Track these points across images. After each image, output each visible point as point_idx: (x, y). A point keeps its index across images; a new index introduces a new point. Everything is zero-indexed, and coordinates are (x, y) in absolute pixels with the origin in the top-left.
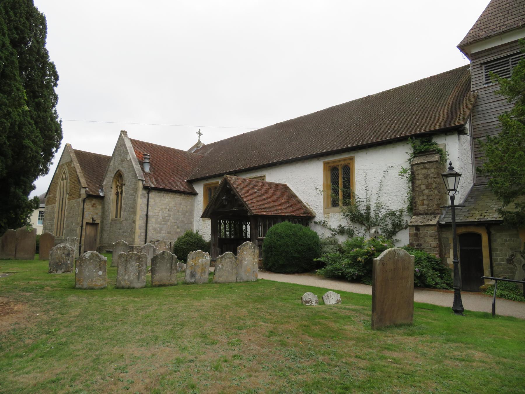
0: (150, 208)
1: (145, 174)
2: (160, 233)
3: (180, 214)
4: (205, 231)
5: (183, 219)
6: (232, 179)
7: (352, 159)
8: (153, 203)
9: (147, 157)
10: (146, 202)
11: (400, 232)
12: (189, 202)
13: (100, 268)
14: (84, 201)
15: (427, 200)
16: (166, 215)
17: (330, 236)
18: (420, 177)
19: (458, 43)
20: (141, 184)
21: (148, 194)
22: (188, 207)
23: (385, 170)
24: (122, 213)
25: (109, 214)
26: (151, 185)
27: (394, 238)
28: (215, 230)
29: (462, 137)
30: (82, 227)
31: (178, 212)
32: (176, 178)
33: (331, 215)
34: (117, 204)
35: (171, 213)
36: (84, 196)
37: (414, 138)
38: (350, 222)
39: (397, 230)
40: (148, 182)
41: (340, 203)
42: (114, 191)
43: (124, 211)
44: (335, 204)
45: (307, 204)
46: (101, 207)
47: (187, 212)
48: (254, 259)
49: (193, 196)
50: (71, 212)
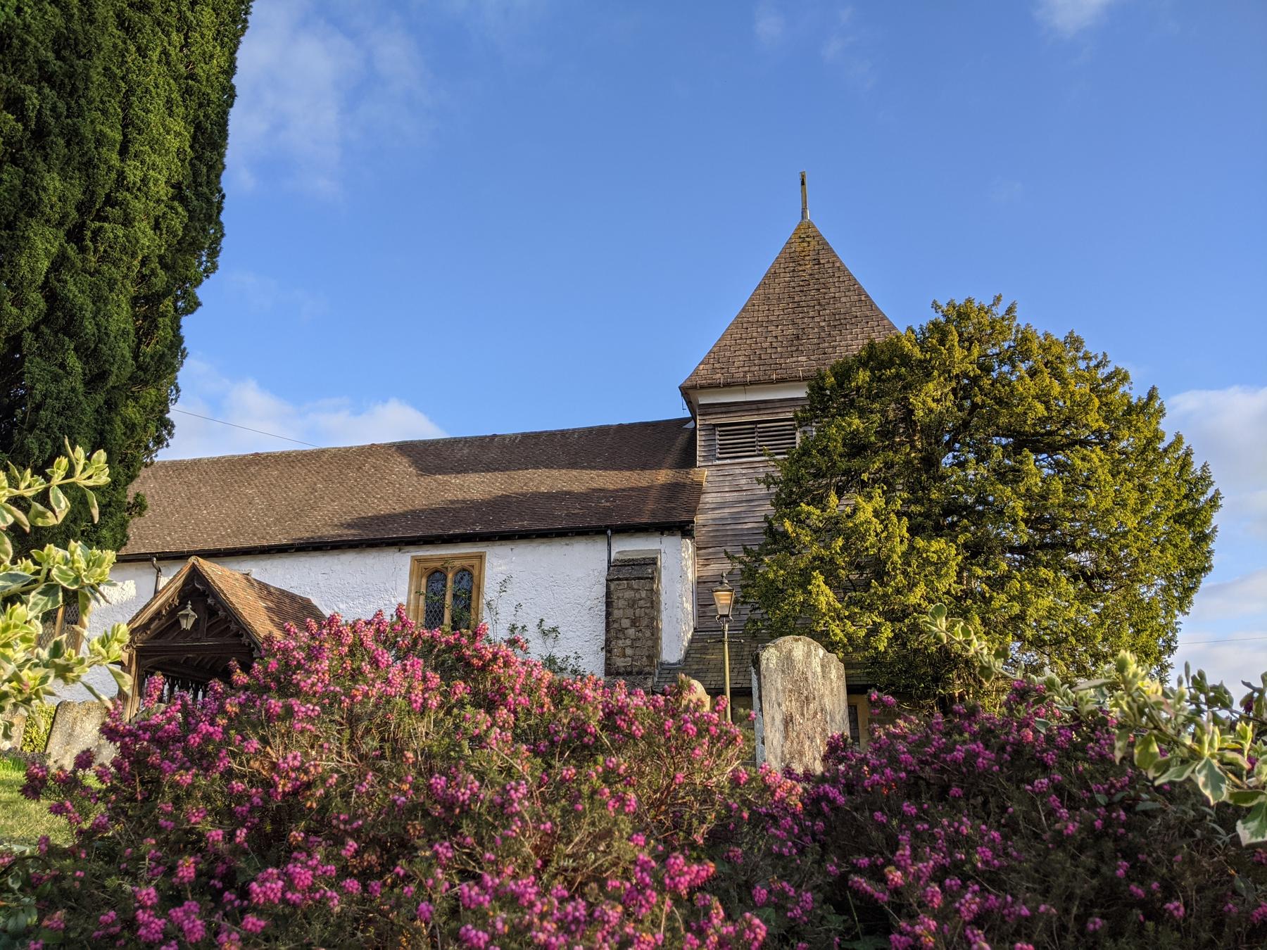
6: (212, 569)
7: (481, 557)
15: (632, 646)
18: (621, 603)
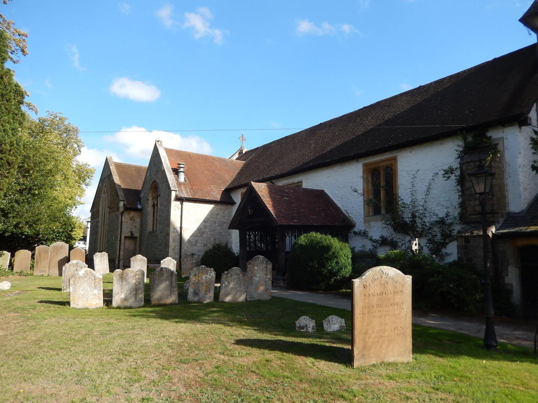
2: (196, 245)
3: (217, 225)
5: (220, 231)
7: (395, 159)
11: (451, 244)
13: (95, 286)
17: (372, 248)
19: (521, 15)
21: (182, 204)
22: (226, 218)
23: (436, 172)
25: (146, 227)
26: (185, 195)
27: (444, 251)
29: (524, 128)
32: (212, 187)
33: (372, 223)
34: (154, 216)
36: (121, 209)
37: (464, 132)
38: (393, 232)
39: (447, 241)
40: (182, 192)
41: (383, 212)
42: (150, 203)
43: (159, 224)
44: (377, 211)
45: (346, 211)
46: (139, 220)
47: (224, 223)
48: (266, 275)
49: (230, 206)
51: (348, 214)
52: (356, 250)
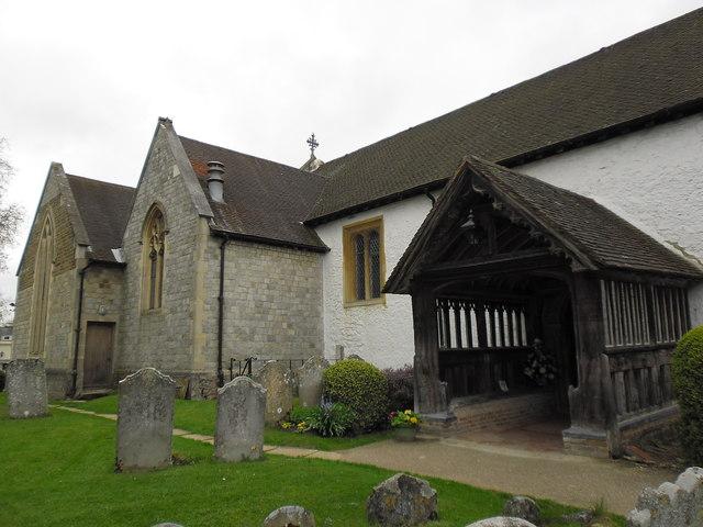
0: (226, 282)
1: (213, 205)
4: (351, 332)
7: (380, 220)
8: (234, 271)
9: (217, 168)
10: (218, 269)
12: (310, 269)
14: (82, 274)
16: (264, 298)
20: (205, 227)
21: (222, 249)
22: (310, 280)
24: (163, 295)
28: (426, 326)
30: (78, 331)
31: (290, 291)
34: (153, 277)
35: (276, 293)
42: (145, 250)
45: (675, 245)
46: (119, 287)
49: (318, 255)
50: (59, 300)
51: (682, 249)
52: (347, 353)
